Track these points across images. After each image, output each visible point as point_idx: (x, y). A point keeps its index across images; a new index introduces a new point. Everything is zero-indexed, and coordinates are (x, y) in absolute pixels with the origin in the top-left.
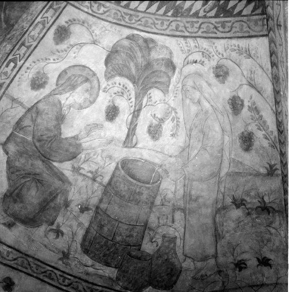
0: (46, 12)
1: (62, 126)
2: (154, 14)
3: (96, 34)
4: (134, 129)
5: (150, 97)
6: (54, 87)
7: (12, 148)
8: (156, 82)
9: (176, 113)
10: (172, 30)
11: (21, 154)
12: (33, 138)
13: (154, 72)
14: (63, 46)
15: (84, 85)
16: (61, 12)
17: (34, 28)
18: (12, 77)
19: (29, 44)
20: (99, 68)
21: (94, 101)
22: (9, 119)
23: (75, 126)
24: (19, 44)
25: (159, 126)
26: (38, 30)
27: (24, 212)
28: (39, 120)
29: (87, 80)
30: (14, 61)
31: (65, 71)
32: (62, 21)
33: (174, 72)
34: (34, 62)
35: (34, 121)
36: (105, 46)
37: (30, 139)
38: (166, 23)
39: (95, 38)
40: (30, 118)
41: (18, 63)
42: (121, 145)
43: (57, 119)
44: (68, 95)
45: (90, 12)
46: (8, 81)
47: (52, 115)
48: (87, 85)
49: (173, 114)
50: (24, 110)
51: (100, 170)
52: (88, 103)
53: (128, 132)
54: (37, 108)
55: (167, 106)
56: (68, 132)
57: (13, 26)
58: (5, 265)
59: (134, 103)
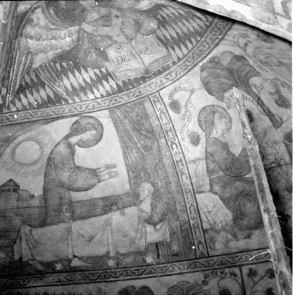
0: (156, 107)
1: (231, 150)
2: (194, 47)
3: (187, 88)
4: (269, 111)
5: (255, 85)
6: (204, 133)
7: (217, 188)
8: (246, 74)
9: (279, 80)
10: (212, 44)
11: (224, 187)
12: (223, 171)
13: (237, 71)
14: (183, 111)
15: (216, 116)
16: (161, 98)
17: (162, 119)
18: (180, 151)
19: (169, 128)
20: (211, 100)
21: (230, 118)
22: (201, 173)
23: (237, 143)
24: (165, 133)
25: (281, 97)
26: (164, 117)
27: (252, 222)
28: (217, 159)
29: (214, 113)
30: (173, 143)
31: (199, 121)
32: (167, 101)
33: (246, 59)
34: (181, 133)
35: (214, 161)
36: (199, 88)
37: (221, 174)
38: (204, 44)
39: (190, 89)
40: (211, 162)
41: (176, 142)
42: (274, 129)
43: (224, 148)
44: (214, 130)
45: (171, 82)
46: (182, 155)
47: (220, 150)
48: (217, 115)
49: (279, 82)
50: (204, 161)
51: (277, 156)
52: (229, 124)
53: (269, 117)
54: (209, 153)
55: (269, 81)
56: (237, 151)
57: (153, 130)
58: (262, 262)
59: (251, 98)
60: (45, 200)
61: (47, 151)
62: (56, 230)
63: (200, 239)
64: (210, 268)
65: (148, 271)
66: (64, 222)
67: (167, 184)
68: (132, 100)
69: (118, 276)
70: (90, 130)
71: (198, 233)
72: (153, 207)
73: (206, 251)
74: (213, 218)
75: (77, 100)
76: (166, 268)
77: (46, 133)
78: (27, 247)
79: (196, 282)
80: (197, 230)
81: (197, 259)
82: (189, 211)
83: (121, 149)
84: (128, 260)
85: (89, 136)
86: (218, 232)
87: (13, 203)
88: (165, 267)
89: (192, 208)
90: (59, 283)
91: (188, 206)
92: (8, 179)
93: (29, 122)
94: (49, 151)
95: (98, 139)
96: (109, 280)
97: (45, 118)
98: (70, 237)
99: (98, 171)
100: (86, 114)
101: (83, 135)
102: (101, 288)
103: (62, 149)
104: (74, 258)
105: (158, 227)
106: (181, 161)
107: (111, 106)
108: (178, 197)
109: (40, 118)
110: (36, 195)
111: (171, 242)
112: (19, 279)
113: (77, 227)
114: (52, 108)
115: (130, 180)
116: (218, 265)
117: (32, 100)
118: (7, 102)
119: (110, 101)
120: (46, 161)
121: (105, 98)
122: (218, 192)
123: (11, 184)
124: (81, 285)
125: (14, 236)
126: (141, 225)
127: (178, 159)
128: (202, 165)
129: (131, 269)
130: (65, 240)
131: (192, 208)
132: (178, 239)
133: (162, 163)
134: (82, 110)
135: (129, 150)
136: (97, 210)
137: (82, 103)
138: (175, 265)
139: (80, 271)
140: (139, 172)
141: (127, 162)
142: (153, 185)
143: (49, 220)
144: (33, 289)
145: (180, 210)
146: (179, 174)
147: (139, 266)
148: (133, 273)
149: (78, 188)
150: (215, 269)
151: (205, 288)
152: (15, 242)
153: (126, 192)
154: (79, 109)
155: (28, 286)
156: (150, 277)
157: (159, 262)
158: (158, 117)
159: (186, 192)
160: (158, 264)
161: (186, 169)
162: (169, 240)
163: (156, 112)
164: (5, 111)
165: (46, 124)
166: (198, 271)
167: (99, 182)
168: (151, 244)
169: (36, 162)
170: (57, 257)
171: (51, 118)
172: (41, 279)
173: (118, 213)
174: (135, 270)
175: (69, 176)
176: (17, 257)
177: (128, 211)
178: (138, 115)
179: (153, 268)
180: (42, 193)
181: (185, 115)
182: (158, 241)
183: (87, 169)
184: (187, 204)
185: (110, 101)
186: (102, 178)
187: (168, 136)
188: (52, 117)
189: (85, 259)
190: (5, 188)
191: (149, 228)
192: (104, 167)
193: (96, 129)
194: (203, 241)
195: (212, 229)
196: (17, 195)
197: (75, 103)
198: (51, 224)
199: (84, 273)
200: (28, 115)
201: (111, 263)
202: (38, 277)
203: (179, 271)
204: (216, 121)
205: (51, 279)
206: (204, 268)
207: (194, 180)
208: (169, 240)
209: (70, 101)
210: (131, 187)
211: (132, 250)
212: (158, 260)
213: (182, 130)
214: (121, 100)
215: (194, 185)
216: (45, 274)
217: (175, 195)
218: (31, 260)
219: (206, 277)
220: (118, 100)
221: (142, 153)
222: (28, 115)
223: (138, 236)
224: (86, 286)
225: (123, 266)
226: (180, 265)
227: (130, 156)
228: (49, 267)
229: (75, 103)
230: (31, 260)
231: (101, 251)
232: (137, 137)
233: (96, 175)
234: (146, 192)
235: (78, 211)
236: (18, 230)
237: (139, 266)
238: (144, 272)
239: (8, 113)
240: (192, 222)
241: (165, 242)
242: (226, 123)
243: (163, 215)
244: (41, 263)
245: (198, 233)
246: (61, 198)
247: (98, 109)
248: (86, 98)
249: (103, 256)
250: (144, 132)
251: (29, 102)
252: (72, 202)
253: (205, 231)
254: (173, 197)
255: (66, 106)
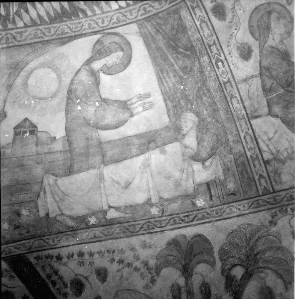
0: (195, 14)
6: (257, 43)
7: (277, 109)
12: (283, 88)
14: (229, 16)
15: (272, 18)
18: (228, 69)
19: (212, 42)
22: (256, 94)
26: (205, 29)
28: (274, 73)
29: (269, 13)
30: (218, 60)
31: (250, 27)
34: (228, 46)
35: (271, 77)
37: (282, 91)
41: (221, 58)
43: (283, 59)
44: (271, 36)
46: (230, 75)
48: (274, 16)
50: (258, 79)
60: (70, 143)
61: (67, 81)
62: (84, 178)
63: (261, 173)
64: (277, 205)
65: (200, 216)
66: (94, 167)
67: (214, 111)
68: (164, 8)
69: (164, 225)
70: (116, 52)
71: (258, 166)
72: (200, 141)
73: (270, 186)
74: (276, 146)
75: (98, 11)
76: (222, 211)
77: (62, 56)
78: (53, 200)
79: (261, 223)
80: (256, 162)
81: (260, 196)
82: (243, 141)
83: (154, 74)
84: (175, 206)
85: (115, 59)
86: (283, 162)
87: (32, 149)
88: (221, 209)
89: (248, 138)
90: (95, 240)
91: (242, 135)
92: (22, 118)
93: (41, 42)
94: (68, 81)
95: (127, 61)
96: (155, 230)
97: (60, 36)
98: (102, 185)
99: (129, 103)
100: (109, 31)
101: (107, 59)
102: (145, 241)
103: (84, 76)
104: (109, 210)
105: (207, 163)
106: (229, 81)
107: (139, 18)
108: (229, 126)
109: (54, 37)
110: (57, 138)
111: (226, 179)
112: (48, 239)
113: (109, 171)
114: (68, 23)
115: (168, 111)
116: (288, 200)
117: (43, 13)
118: (11, 13)
119: (139, 11)
120: (66, 93)
121: (131, 8)
122: (279, 114)
123: (27, 124)
124: (121, 240)
125: (36, 188)
126: (186, 164)
127: (226, 80)
128: (257, 82)
129: (179, 215)
130: (98, 189)
131: (248, 138)
132: (234, 175)
133: (206, 86)
134: (104, 25)
135: (165, 75)
136: (132, 150)
137: (104, 15)
138: (233, 206)
139: (118, 223)
140: (179, 101)
141: (163, 89)
142: (197, 114)
143: (76, 167)
144: (65, 248)
145: (233, 142)
146: (229, 98)
147: (188, 212)
148: (182, 220)
149: (107, 125)
150: (283, 206)
151: (274, 229)
152: (39, 196)
153: (164, 126)
154: (100, 25)
155: (58, 246)
156: (203, 223)
157: (213, 204)
158: (198, 28)
159: (239, 119)
160: (212, 207)
161: (236, 92)
162: (222, 178)
163: (195, 23)
164: (10, 26)
165: (63, 43)
166: (263, 210)
167: (132, 116)
168: (200, 185)
169: (54, 96)
170: (89, 210)
171: (68, 37)
172: (73, 237)
173: (157, 151)
174: (185, 217)
175: (96, 111)
176: (42, 214)
177: (169, 148)
178: (173, 28)
179: (205, 212)
180: (65, 135)
181: (232, 22)
182: (209, 179)
183: (116, 101)
184: (240, 132)
185: (139, 11)
186: (135, 112)
187: (212, 52)
188: (69, 35)
189: (122, 209)
190: (19, 130)
191: (197, 166)
192: (136, 98)
193: (122, 50)
194: (265, 174)
195: (275, 159)
196: (35, 139)
197: (95, 15)
198: (79, 171)
199: (123, 225)
200: (39, 32)
201: (154, 211)
202: (70, 235)
203: (239, 213)
204: (273, 25)
205: (84, 236)
206: (270, 206)
207: (247, 104)
208: (222, 178)
209: (89, 13)
210: (171, 120)
211: (177, 194)
212: (211, 203)
213: (228, 42)
214: (151, 9)
215: (247, 109)
216: (77, 230)
217: (225, 123)
218: (59, 215)
219: (273, 217)
220: (148, 9)
221: (181, 77)
222: (39, 32)
223: (184, 176)
224: (127, 240)
225: (169, 213)
226: (239, 205)
227: (167, 82)
228: (82, 222)
229: (95, 15)
230: (59, 215)
231: (140, 198)
232: (173, 58)
233: (128, 109)
234: (190, 125)
235: (109, 154)
236: (40, 181)
237: (188, 212)
238: (195, 217)
239: (14, 29)
240: (249, 154)
241: (217, 181)
242: (285, 25)
243: (212, 149)
244: (71, 217)
245: (258, 166)
246: (88, 139)
247: (125, 23)
248: (108, 9)
249: (143, 204)
250: (181, 50)
251: (39, 15)
252: (101, 143)
253: (267, 163)
254: (223, 126)
255: (84, 20)
